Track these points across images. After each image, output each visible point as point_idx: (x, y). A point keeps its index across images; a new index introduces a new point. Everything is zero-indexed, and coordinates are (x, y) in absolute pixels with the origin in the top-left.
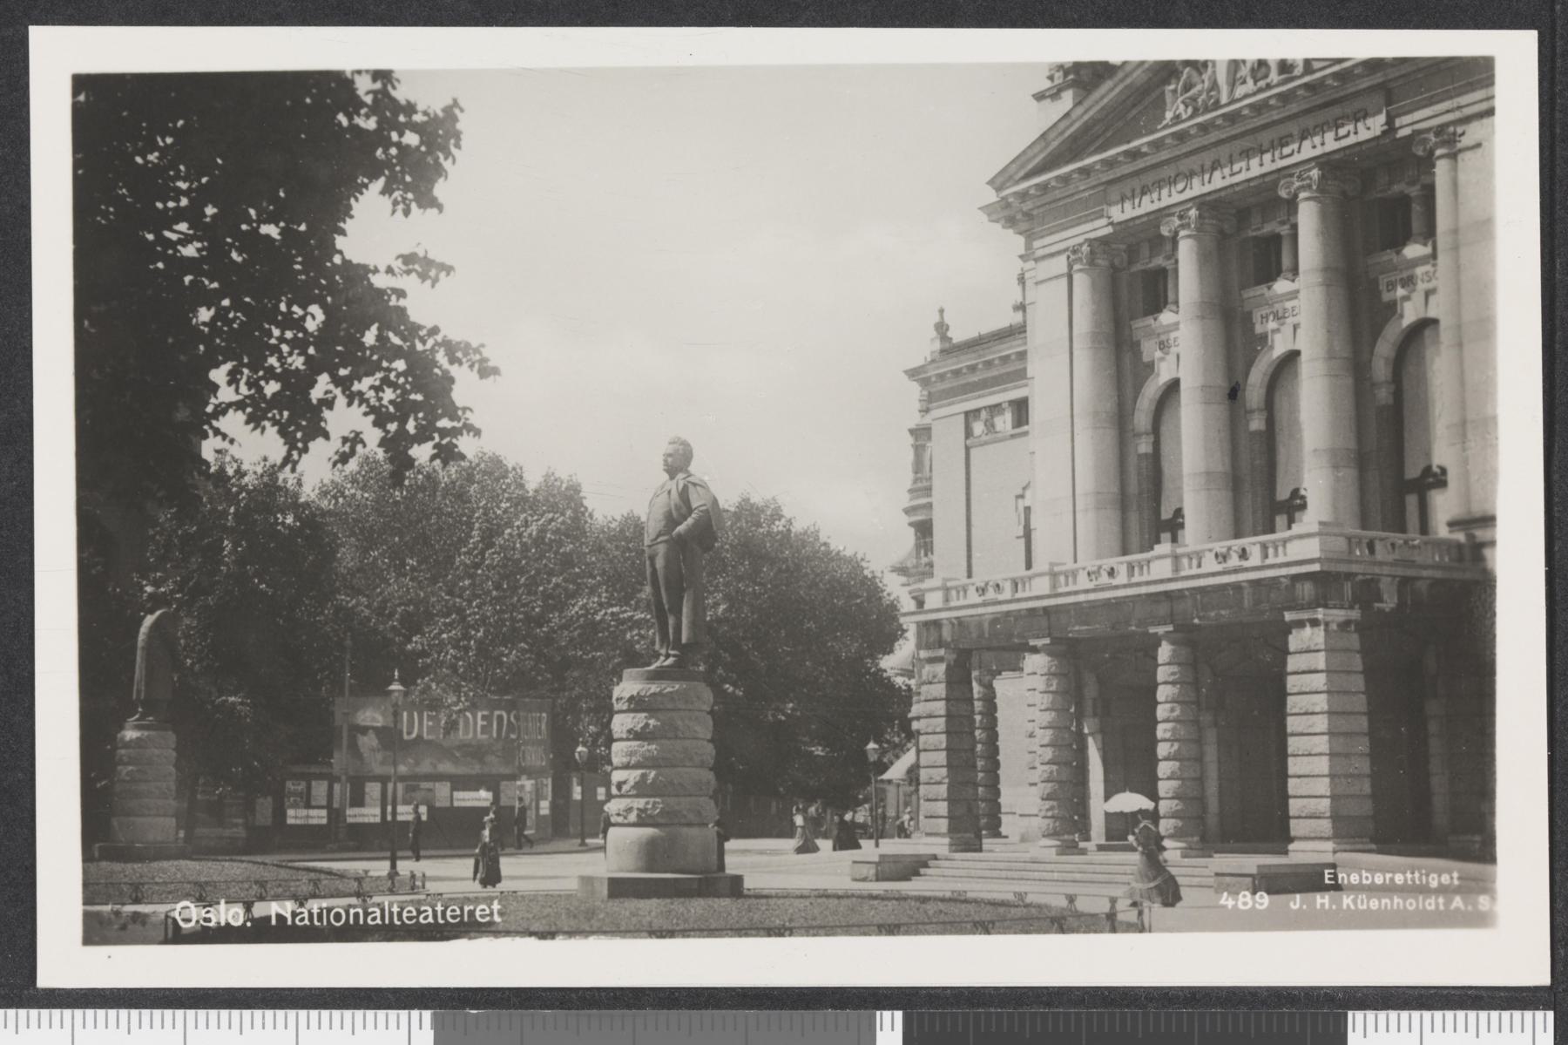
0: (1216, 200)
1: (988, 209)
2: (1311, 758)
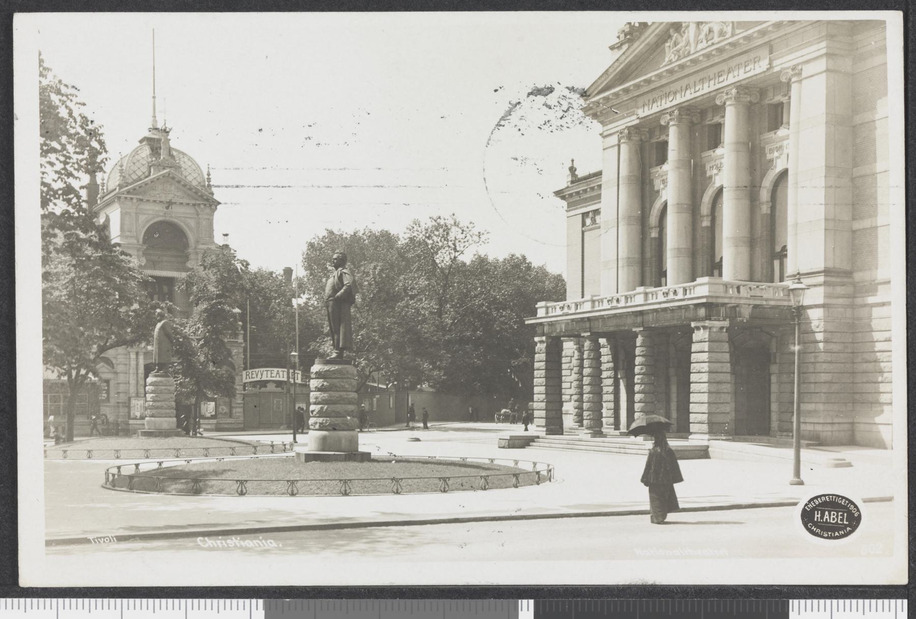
0: (688, 106)
2: (700, 394)
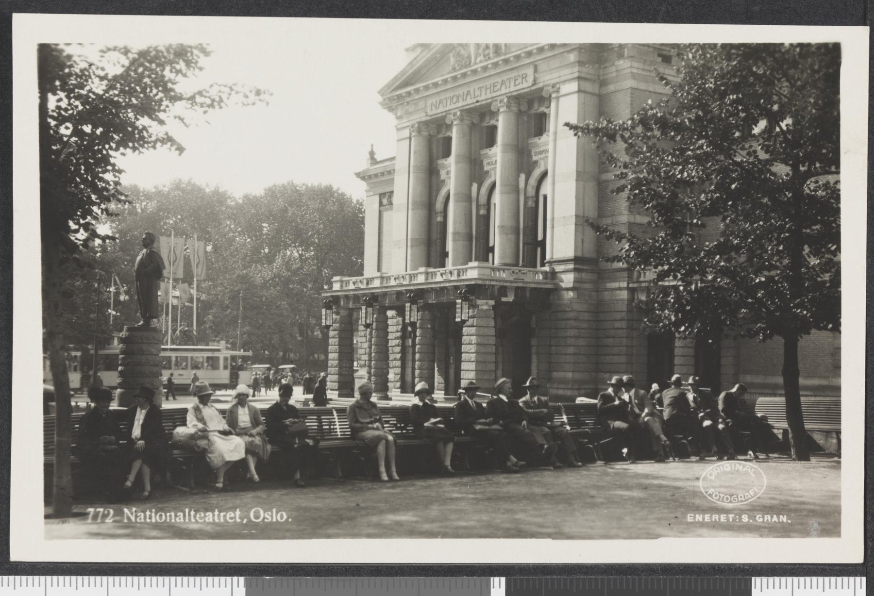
0: (518, 95)
1: (382, 104)
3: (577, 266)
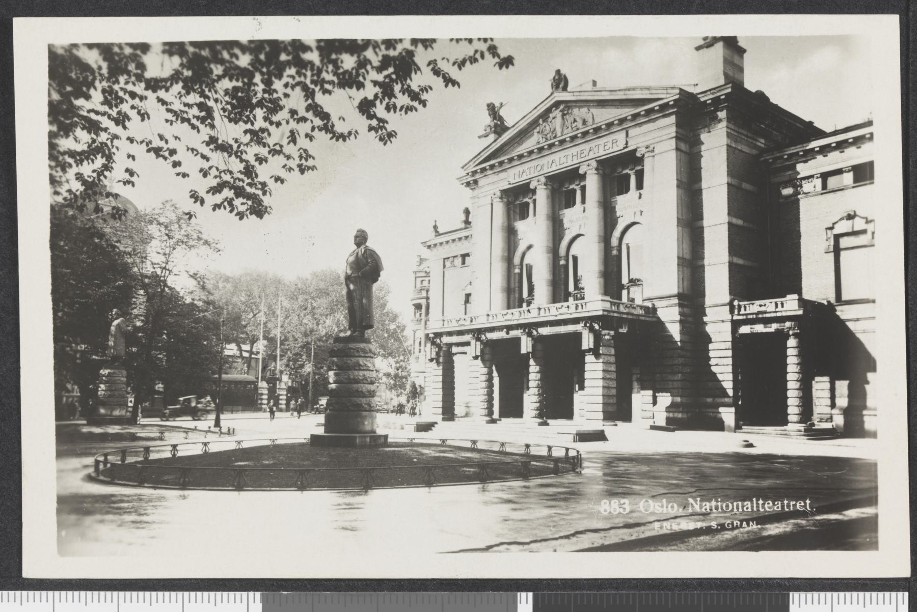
3: (681, 302)
